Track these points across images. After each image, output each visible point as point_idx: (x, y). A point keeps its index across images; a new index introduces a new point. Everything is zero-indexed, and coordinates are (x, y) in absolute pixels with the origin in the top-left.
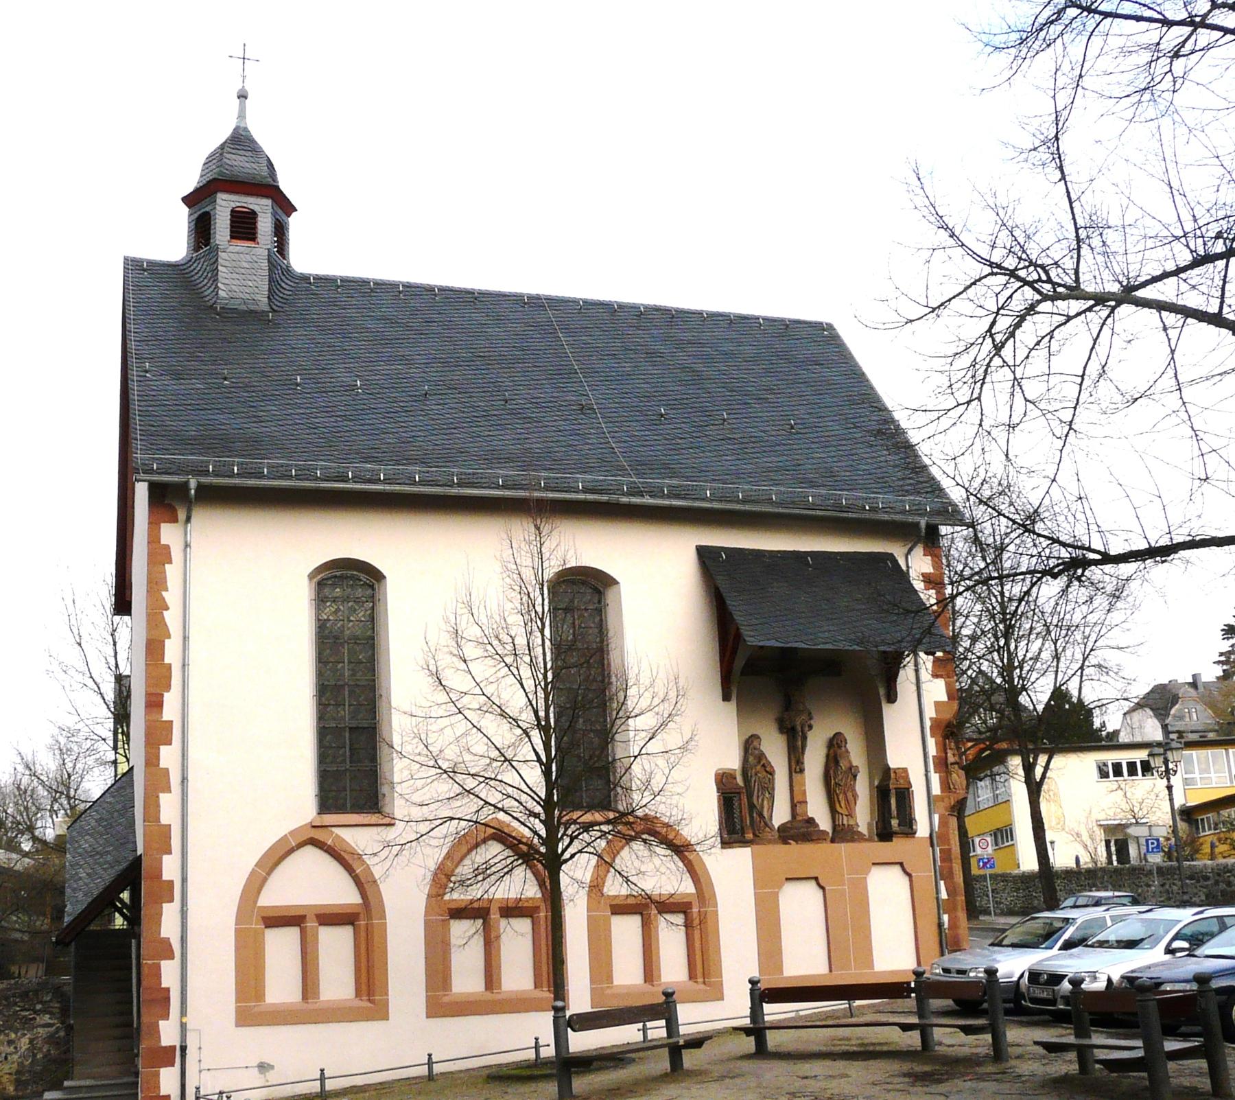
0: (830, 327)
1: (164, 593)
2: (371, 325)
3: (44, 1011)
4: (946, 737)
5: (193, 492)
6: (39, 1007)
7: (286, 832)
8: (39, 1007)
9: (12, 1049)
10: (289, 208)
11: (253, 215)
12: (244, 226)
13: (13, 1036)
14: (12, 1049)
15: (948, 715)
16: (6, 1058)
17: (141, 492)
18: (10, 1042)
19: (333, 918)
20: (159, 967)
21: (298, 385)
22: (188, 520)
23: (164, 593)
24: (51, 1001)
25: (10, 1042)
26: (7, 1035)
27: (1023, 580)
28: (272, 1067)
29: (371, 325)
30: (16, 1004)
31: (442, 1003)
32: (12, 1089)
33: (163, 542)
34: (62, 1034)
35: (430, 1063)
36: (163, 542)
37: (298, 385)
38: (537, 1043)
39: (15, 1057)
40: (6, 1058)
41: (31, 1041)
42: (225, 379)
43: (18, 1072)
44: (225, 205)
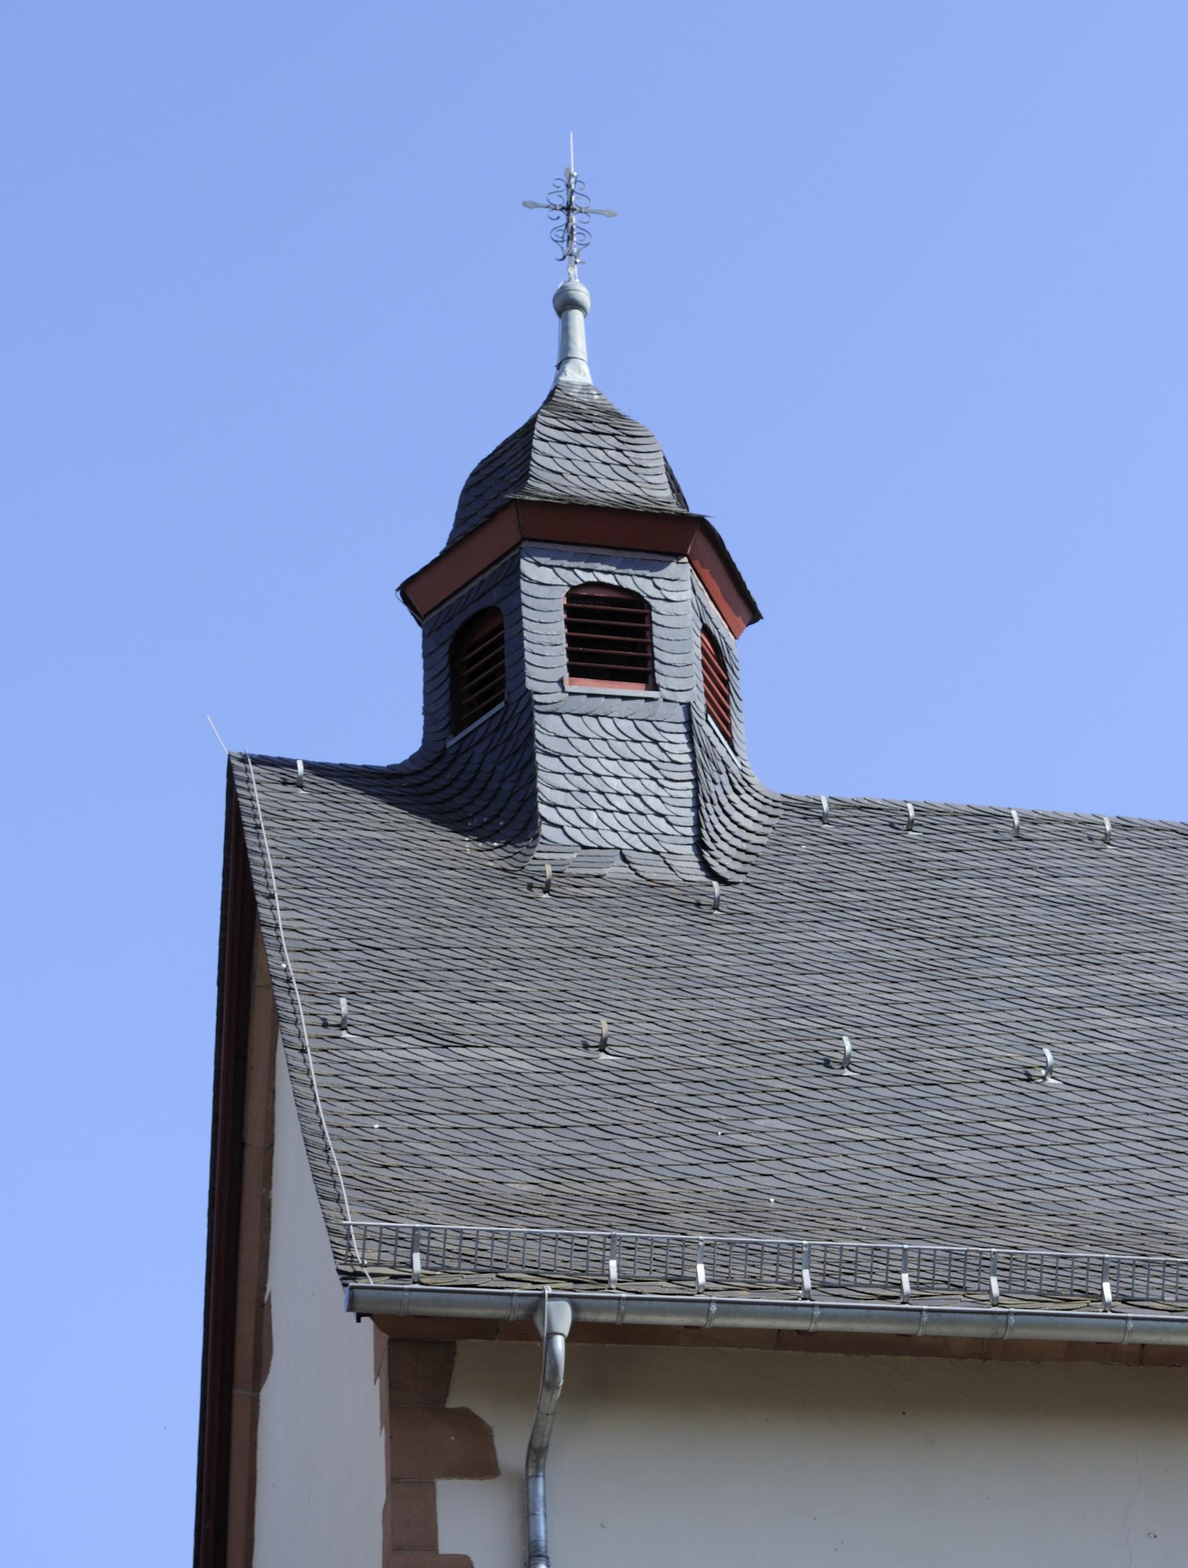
12: (612, 641)
36: (448, 1544)
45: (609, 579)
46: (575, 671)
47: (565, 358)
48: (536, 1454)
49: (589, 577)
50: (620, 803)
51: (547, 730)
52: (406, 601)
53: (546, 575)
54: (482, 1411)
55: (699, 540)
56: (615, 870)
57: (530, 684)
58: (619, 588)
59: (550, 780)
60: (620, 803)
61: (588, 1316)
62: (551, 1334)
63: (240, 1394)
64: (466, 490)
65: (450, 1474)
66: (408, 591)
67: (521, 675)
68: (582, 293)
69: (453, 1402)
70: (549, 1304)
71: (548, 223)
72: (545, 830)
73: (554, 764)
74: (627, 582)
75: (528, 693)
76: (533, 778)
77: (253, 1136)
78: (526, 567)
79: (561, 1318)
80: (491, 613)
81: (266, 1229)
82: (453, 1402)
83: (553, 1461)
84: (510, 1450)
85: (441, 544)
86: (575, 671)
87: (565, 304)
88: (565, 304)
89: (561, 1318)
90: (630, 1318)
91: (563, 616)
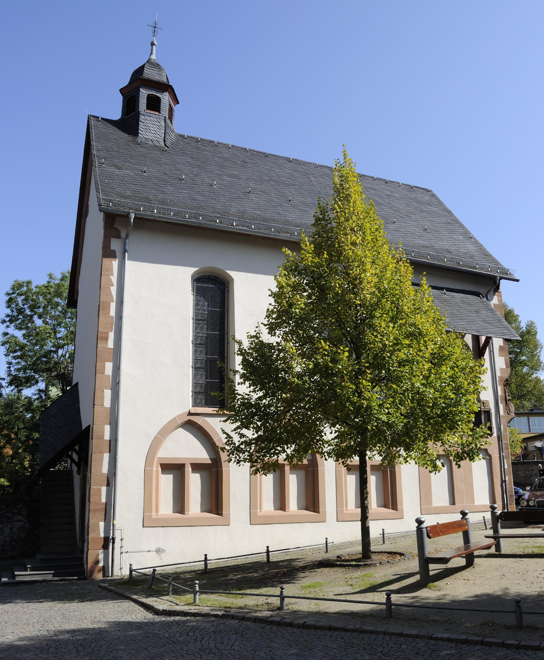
2: (216, 159)
4: (505, 386)
5: (132, 220)
6: (15, 511)
8: (15, 511)
10: (177, 102)
11: (158, 100)
12: (154, 104)
15: (506, 376)
17: (95, 222)
19: (197, 467)
21: (183, 180)
22: (127, 236)
28: (164, 551)
29: (216, 159)
31: (255, 519)
33: (112, 248)
34: (27, 525)
35: (206, 560)
36: (112, 248)
37: (183, 180)
38: (206, 558)
42: (145, 172)
44: (144, 93)
46: (147, 109)
47: (151, 54)
50: (152, 132)
51: (142, 118)
52: (121, 92)
53: (144, 91)
55: (170, 89)
56: (150, 143)
60: (152, 132)
63: (83, 219)
65: (113, 237)
68: (156, 43)
69: (115, 226)
71: (151, 29)
72: (140, 135)
73: (142, 124)
74: (157, 95)
75: (139, 111)
78: (141, 89)
79: (133, 216)
82: (115, 226)
84: (123, 235)
86: (147, 109)
87: (153, 44)
88: (153, 44)
89: (133, 216)
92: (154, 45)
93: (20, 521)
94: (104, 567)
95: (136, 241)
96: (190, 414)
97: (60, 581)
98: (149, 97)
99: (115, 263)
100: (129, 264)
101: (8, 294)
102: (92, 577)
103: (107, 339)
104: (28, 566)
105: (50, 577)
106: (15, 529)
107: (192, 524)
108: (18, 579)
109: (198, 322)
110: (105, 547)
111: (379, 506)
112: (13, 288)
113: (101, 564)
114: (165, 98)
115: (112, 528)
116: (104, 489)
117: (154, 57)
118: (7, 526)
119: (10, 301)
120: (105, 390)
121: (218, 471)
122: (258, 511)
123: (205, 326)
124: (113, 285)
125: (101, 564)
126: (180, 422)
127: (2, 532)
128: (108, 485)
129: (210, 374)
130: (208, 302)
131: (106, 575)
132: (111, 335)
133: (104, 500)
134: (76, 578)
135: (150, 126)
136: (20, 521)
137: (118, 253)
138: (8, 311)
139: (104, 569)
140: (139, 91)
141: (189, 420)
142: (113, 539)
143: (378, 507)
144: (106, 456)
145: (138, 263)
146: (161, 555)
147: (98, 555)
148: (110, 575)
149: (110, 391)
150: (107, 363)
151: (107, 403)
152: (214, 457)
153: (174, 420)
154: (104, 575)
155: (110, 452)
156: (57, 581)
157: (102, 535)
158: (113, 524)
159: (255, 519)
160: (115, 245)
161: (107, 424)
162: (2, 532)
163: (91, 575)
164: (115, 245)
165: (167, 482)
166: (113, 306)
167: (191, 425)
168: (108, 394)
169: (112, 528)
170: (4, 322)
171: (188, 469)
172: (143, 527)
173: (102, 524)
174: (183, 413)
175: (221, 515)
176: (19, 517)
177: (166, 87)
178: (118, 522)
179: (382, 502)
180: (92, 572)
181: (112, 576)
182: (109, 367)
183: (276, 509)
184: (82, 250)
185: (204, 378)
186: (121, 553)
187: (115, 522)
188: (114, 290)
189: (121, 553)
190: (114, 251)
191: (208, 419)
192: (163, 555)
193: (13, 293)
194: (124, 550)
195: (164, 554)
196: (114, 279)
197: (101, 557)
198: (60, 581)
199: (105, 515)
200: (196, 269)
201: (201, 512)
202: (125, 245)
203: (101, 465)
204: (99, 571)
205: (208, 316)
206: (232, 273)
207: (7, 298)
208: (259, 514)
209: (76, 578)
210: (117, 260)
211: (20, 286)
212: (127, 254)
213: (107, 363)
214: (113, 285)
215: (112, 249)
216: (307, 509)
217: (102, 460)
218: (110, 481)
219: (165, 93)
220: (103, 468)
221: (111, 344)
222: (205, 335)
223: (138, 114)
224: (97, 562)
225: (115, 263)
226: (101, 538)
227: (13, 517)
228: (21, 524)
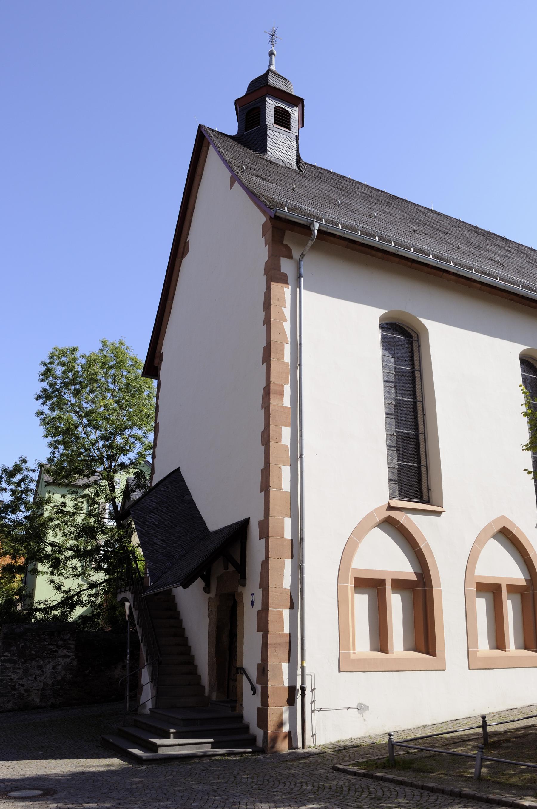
0: (264, 348)
1: (283, 309)
3: (66, 647)
6: (60, 643)
7: (372, 510)
8: (60, 643)
9: (40, 672)
11: (287, 115)
12: (283, 119)
13: (42, 663)
14: (40, 672)
16: (35, 678)
18: (39, 667)
19: (400, 585)
20: (262, 705)
23: (283, 309)
24: (69, 639)
25: (39, 667)
26: (37, 661)
27: (98, 476)
30: (45, 640)
31: (474, 663)
32: (38, 701)
34: (75, 663)
36: (283, 270)
39: (42, 678)
40: (35, 678)
41: (54, 667)
43: (43, 689)
45: (283, 107)
46: (275, 123)
47: (270, 64)
48: (303, 255)
49: (279, 105)
50: (282, 151)
51: (269, 132)
52: (235, 103)
53: (271, 102)
54: (290, 246)
55: (300, 105)
56: (281, 164)
57: (267, 123)
58: (285, 109)
59: (270, 143)
60: (282, 151)
61: (321, 228)
62: (315, 229)
63: (178, 260)
64: (250, 85)
65: (283, 257)
66: (237, 102)
67: (265, 121)
68: (275, 53)
69: (284, 242)
70: (315, 223)
71: (269, 37)
72: (268, 152)
73: (271, 140)
74: (286, 108)
75: (267, 125)
76: (267, 142)
77: (190, 207)
78: (267, 99)
79: (317, 226)
80: (258, 108)
81: (190, 227)
82: (284, 242)
83: (305, 258)
84: (296, 254)
85: (243, 94)
86: (275, 123)
87: (271, 54)
88: (271, 54)
89: (317, 226)
90: (329, 231)
91: (273, 111)
92: (274, 54)
93: (66, 656)
94: (289, 733)
95: (314, 264)
96: (390, 508)
97: (229, 754)
98: (277, 110)
99: (287, 291)
100: (306, 295)
101: (44, 364)
102: (275, 749)
103: (281, 394)
104: (172, 730)
105: (207, 749)
106: (60, 667)
107: (398, 668)
108: (162, 751)
109: (388, 384)
110: (291, 702)
111: (517, 648)
112: (52, 357)
113: (286, 728)
114: (294, 113)
115: (299, 672)
116: (286, 613)
117: (273, 68)
118: (49, 662)
119: (47, 373)
120: (283, 467)
121: (425, 591)
122: (351, 652)
123: (393, 390)
124: (286, 321)
125: (286, 728)
126: (378, 519)
127: (43, 671)
128: (292, 606)
129: (402, 455)
130: (394, 358)
131: (294, 746)
132: (287, 389)
133: (286, 630)
134: (250, 750)
135: (280, 145)
136: (66, 656)
137: (291, 277)
138: (45, 385)
139: (290, 736)
140: (266, 100)
141: (389, 517)
142: (303, 689)
143: (406, 649)
144: (288, 563)
145: (315, 294)
146: (364, 714)
147: (282, 714)
148: (300, 745)
149: (289, 468)
150: (283, 428)
151: (286, 486)
152: (419, 571)
153: (371, 514)
154: (291, 747)
155: (292, 558)
156: (223, 755)
157: (286, 684)
158: (303, 667)
159: (474, 663)
160: (286, 266)
161: (287, 516)
162: (43, 671)
163: (273, 747)
164: (286, 266)
165: (361, 603)
166: (287, 348)
167: (392, 526)
168: (286, 471)
169: (299, 672)
170: (38, 398)
171: (389, 587)
172: (340, 671)
173: (285, 667)
174: (381, 507)
175: (434, 654)
176: (65, 651)
177: (297, 101)
178: (310, 664)
179: (494, 644)
180: (275, 739)
181: (303, 747)
182: (286, 433)
183: (373, 649)
184: (172, 300)
185: (396, 459)
186: (313, 711)
187: (305, 664)
188: (287, 326)
189: (313, 711)
190: (285, 275)
191: (413, 517)
192: (366, 714)
193: (51, 363)
194: (317, 706)
195: (367, 712)
196: (287, 312)
197: (286, 716)
198: (229, 754)
199: (289, 652)
200: (385, 311)
201: (490, 649)
202: (299, 268)
203: (282, 576)
204: (285, 737)
205: (395, 377)
206: (426, 322)
207: (44, 369)
208: (352, 656)
209: (250, 750)
210: (290, 287)
211: (63, 353)
212: (302, 279)
213: (283, 428)
214: (286, 321)
215: (282, 271)
216: (416, 650)
217: (282, 569)
218: (295, 600)
219: (295, 108)
220: (284, 581)
221: (287, 402)
222: (394, 403)
223: (265, 128)
224: (281, 725)
225: (287, 291)
226: (285, 687)
227: (57, 651)
228: (68, 660)
